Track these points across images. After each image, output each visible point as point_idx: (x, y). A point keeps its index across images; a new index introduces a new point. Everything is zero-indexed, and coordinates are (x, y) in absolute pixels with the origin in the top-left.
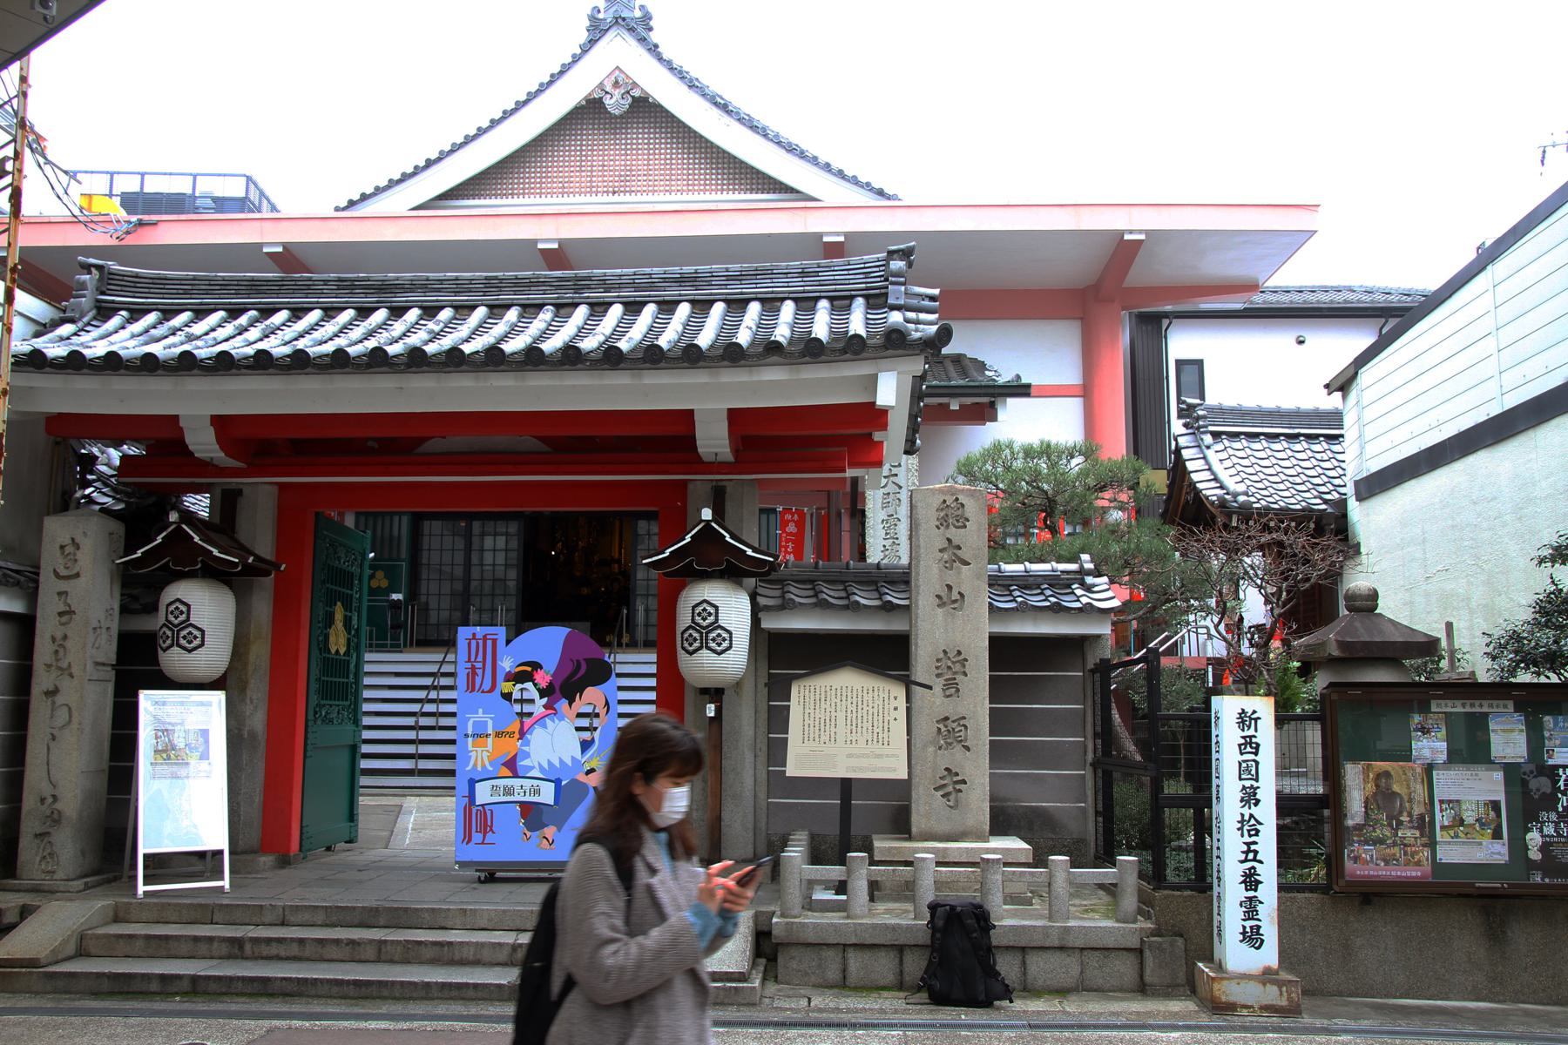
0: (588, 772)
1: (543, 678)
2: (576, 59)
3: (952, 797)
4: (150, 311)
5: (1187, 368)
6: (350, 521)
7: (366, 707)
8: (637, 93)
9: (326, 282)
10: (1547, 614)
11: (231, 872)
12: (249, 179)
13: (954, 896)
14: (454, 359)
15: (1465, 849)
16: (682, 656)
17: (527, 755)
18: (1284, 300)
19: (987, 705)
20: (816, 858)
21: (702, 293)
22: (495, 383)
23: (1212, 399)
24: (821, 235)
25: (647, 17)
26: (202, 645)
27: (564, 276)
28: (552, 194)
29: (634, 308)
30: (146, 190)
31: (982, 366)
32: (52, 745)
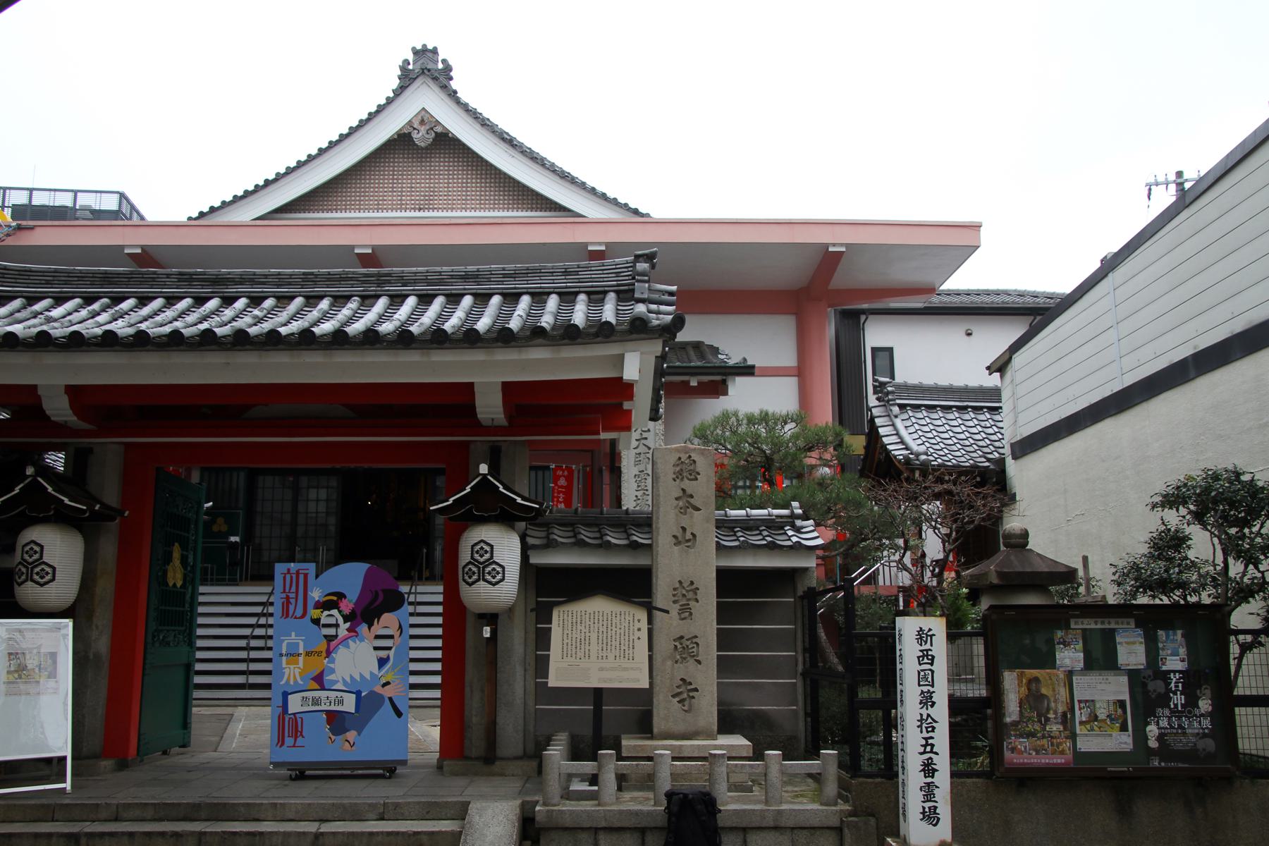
0: (384, 685)
1: (347, 605)
2: (390, 101)
3: (686, 703)
4: (16, 298)
5: (880, 354)
6: (195, 477)
7: (200, 632)
8: (439, 129)
9: (168, 276)
10: (1159, 548)
11: (73, 775)
12: (122, 196)
13: (685, 786)
14: (273, 340)
15: (1100, 739)
16: (463, 587)
17: (333, 671)
18: (956, 301)
19: (715, 626)
20: (576, 753)
21: (483, 288)
22: (308, 360)
23: (899, 379)
24: (586, 244)
25: (448, 69)
26: (53, 579)
27: (374, 274)
28: (369, 210)
29: (425, 300)
30: (35, 202)
31: (715, 351)
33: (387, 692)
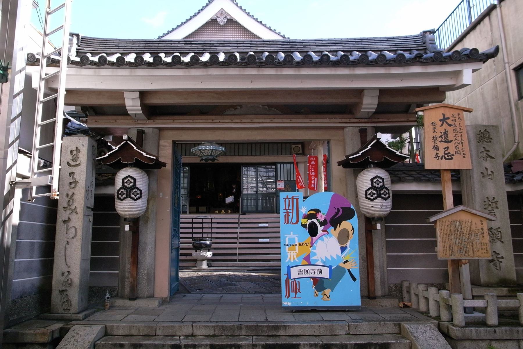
1: (321, 217)
8: (229, 17)
17: (315, 254)
32: (67, 246)
33: (347, 266)
